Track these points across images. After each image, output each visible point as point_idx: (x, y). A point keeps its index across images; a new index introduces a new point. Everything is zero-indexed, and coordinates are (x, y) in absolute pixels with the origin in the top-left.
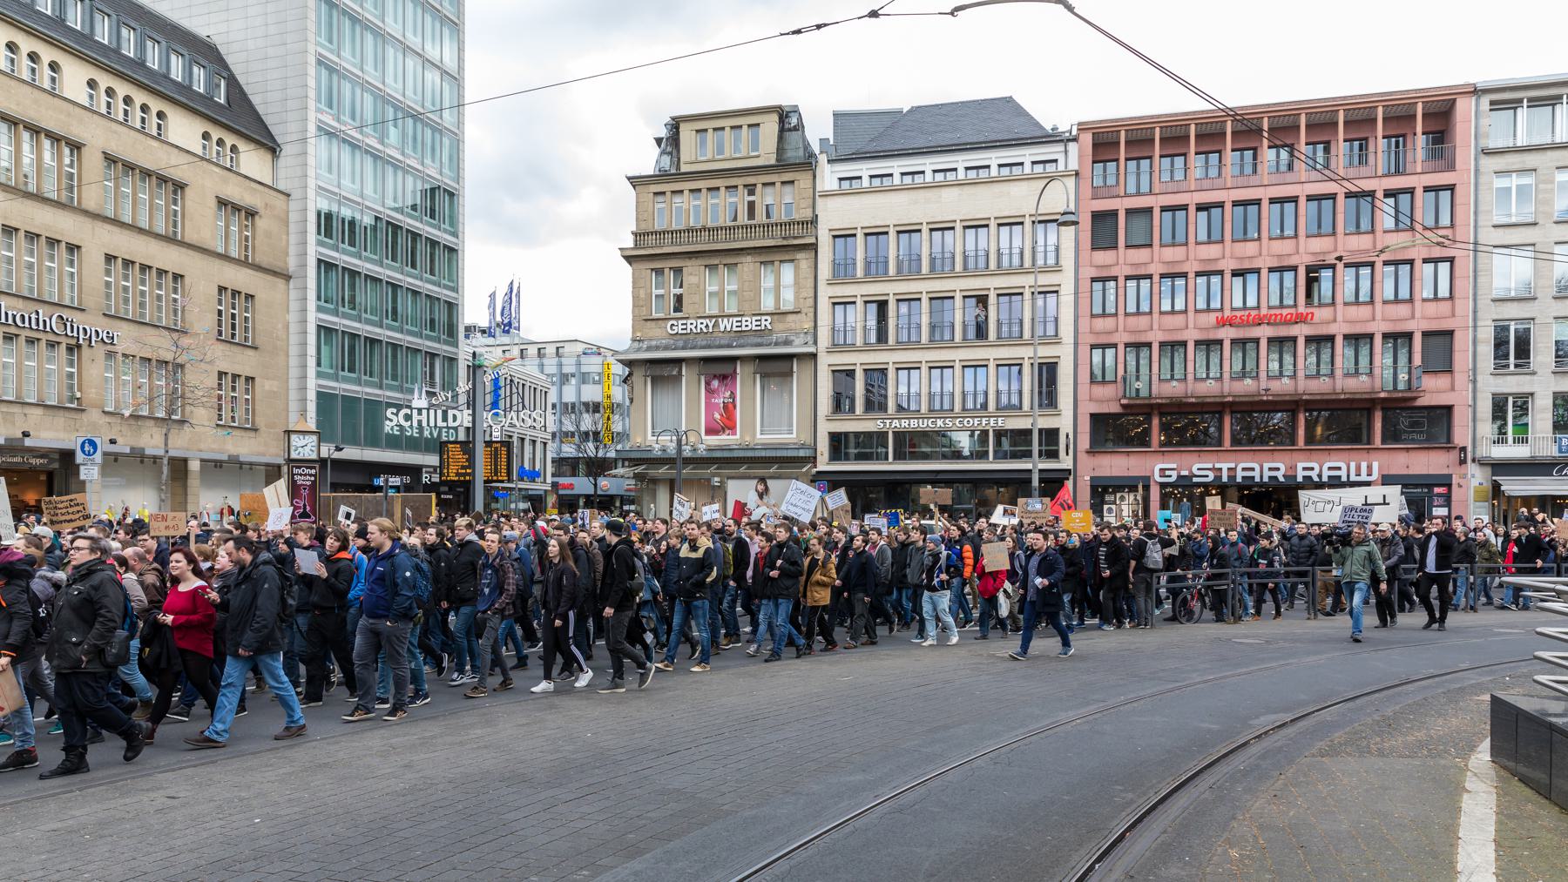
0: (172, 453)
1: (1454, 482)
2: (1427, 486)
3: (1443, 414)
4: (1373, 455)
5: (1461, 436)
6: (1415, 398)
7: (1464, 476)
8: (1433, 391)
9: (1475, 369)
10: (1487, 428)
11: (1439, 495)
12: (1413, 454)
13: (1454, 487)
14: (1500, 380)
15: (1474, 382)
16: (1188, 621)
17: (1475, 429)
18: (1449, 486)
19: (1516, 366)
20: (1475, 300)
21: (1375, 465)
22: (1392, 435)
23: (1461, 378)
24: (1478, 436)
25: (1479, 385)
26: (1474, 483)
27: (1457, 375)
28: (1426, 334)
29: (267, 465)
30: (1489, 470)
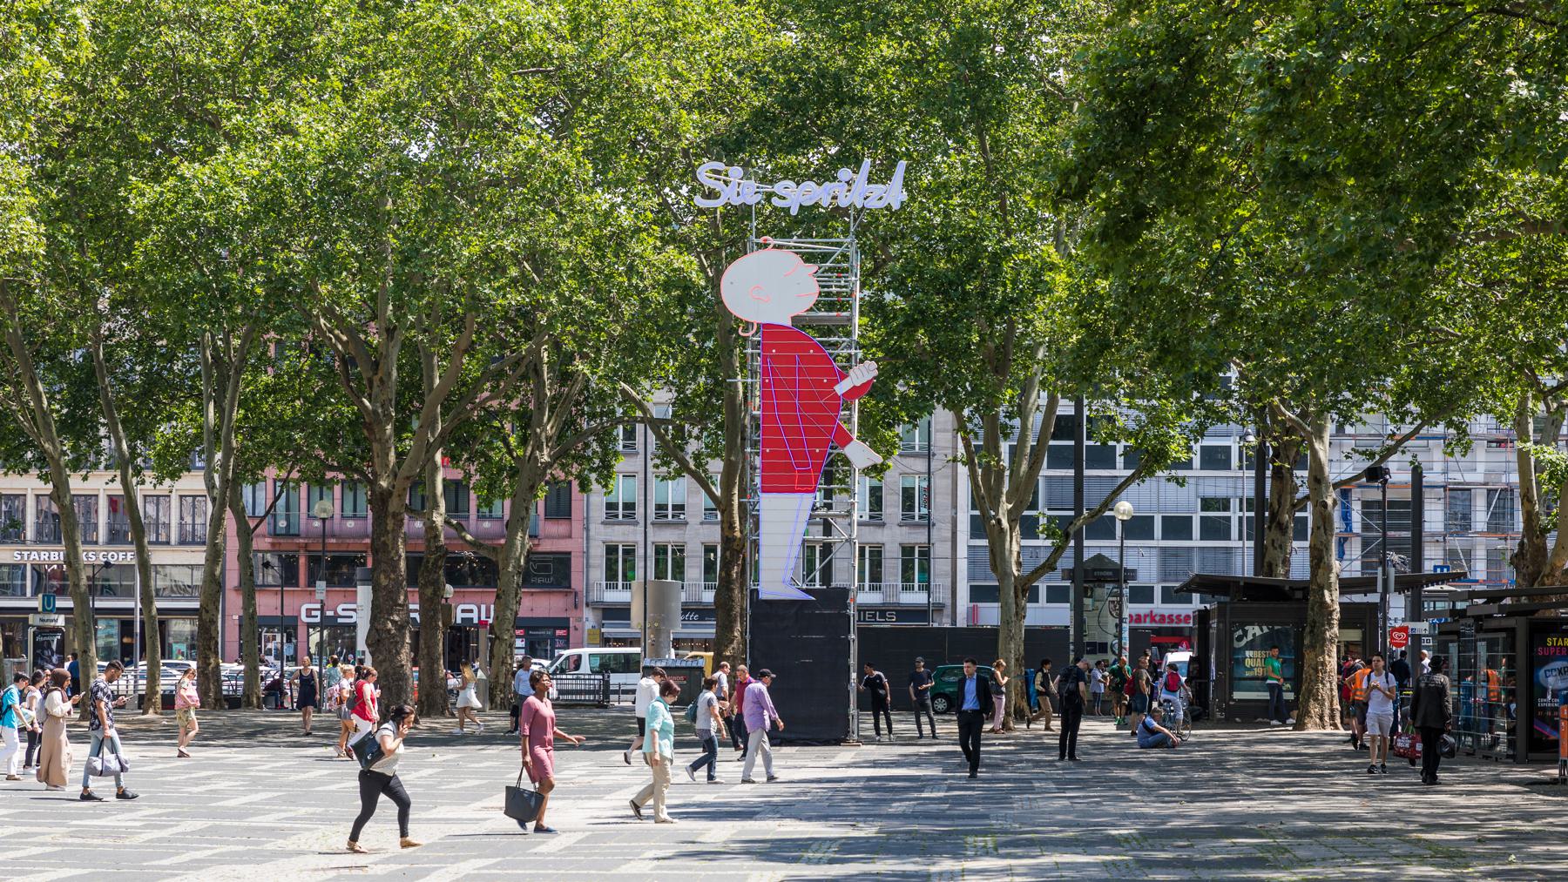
5: (577, 582)
7: (580, 619)
10: (598, 574)
11: (560, 637)
12: (536, 598)
14: (610, 529)
15: (588, 530)
17: (591, 575)
18: (567, 628)
23: (577, 527)
25: (592, 533)
26: (588, 625)
30: (600, 613)
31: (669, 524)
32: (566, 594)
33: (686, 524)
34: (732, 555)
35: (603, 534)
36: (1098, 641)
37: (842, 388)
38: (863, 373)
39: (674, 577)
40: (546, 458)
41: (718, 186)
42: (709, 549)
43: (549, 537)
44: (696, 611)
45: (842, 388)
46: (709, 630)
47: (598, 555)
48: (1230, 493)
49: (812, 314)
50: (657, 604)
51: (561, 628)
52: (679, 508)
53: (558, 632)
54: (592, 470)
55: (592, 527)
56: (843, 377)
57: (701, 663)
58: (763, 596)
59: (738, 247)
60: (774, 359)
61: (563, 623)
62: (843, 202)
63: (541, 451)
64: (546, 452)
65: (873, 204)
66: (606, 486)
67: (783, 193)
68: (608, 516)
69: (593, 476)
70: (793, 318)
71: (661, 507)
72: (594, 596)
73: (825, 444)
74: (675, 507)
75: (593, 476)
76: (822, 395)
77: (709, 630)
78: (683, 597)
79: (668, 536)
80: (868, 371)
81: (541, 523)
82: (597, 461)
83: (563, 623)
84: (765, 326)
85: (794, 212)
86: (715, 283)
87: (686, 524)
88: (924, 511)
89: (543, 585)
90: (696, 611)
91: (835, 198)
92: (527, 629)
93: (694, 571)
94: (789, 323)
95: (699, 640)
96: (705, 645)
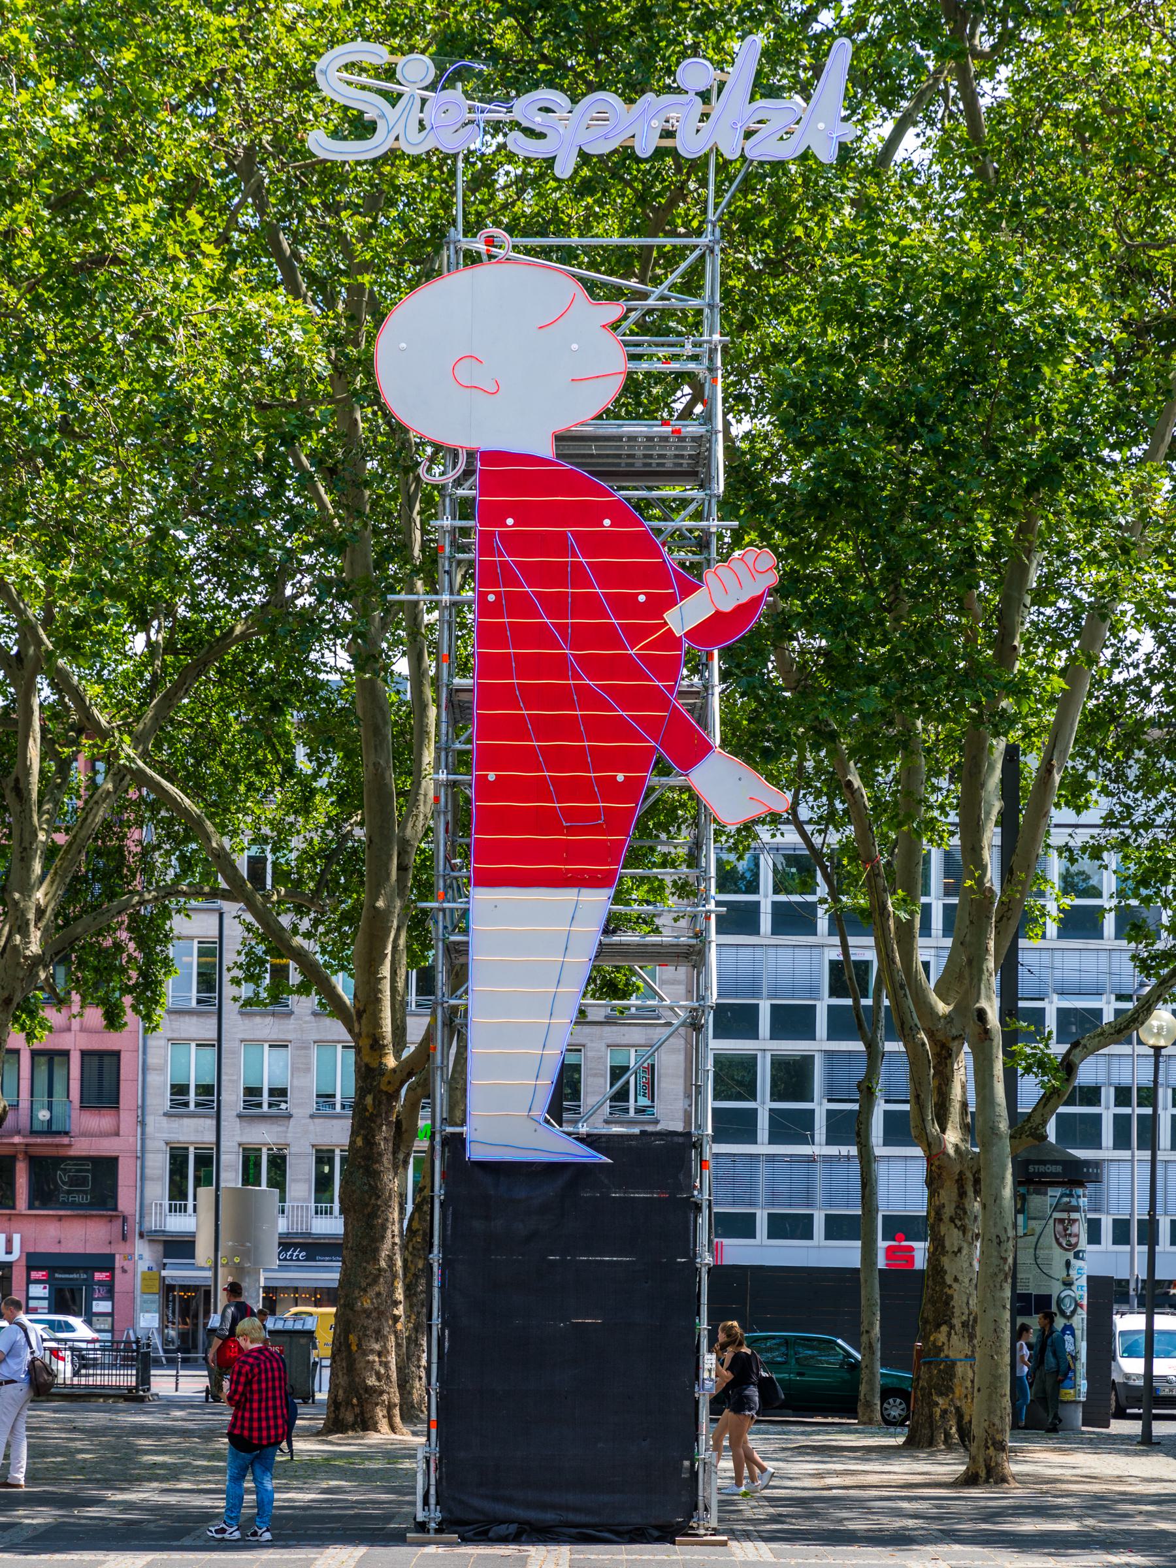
0: (1127, 1248)
1: (117, 1265)
2: (86, 1269)
3: (106, 1167)
4: (15, 1224)
5: (126, 1201)
6: (70, 1145)
7: (129, 1257)
8: (89, 1135)
9: (143, 1107)
10: (158, 1191)
11: (101, 1283)
12: (66, 1224)
13: (118, 1272)
14: (176, 1123)
15: (143, 1124)
16: (466, 953)
17: (146, 1191)
18: (111, 1269)
19: (197, 1105)
20: (144, 1053)
21: (17, 1238)
22: (42, 1196)
23: (127, 1118)
24: (147, 1202)
25: (149, 1129)
26: (142, 1266)
27: (123, 1114)
28: (84, 1054)
29: (317, 1191)
30: (160, 1248)
31: (264, 1117)
32: (111, 1219)
33: (290, 1116)
34: (377, 1103)
35: (167, 1130)
36: (1034, 1291)
37: (683, 618)
38: (741, 578)
39: (271, 1184)
40: (35, 948)
41: (372, 106)
42: (323, 1157)
43: (84, 1134)
44: (303, 1246)
45: (683, 618)
46: (329, 1275)
47: (159, 1164)
48: (1101, 1078)
49: (610, 428)
50: (241, 1227)
51: (101, 1269)
52: (279, 1093)
53: (99, 1276)
54: (127, 990)
55: (150, 1120)
56: (688, 589)
57: (310, 1324)
58: (476, 1153)
59: (425, 257)
60: (513, 542)
61: (106, 1263)
62: (690, 146)
63: (25, 934)
64: (36, 935)
65: (765, 149)
66: (148, 1017)
67: (538, 121)
68: (175, 1104)
69: (128, 1000)
70: (560, 438)
71: (252, 1092)
72: (152, 1223)
73: (637, 760)
74: (272, 1092)
75: (128, 1000)
76: (636, 633)
77: (329, 1275)
78: (282, 1225)
79: (264, 1135)
80: (754, 572)
81: (75, 1113)
82: (134, 974)
83: (106, 1263)
84: (491, 457)
85: (565, 168)
86: (354, 369)
87: (290, 1116)
88: (644, 1101)
89: (73, 1206)
90: (303, 1246)
91: (668, 134)
92: (51, 1270)
93: (300, 1186)
94: (546, 450)
95: (306, 1290)
96: (321, 1296)
